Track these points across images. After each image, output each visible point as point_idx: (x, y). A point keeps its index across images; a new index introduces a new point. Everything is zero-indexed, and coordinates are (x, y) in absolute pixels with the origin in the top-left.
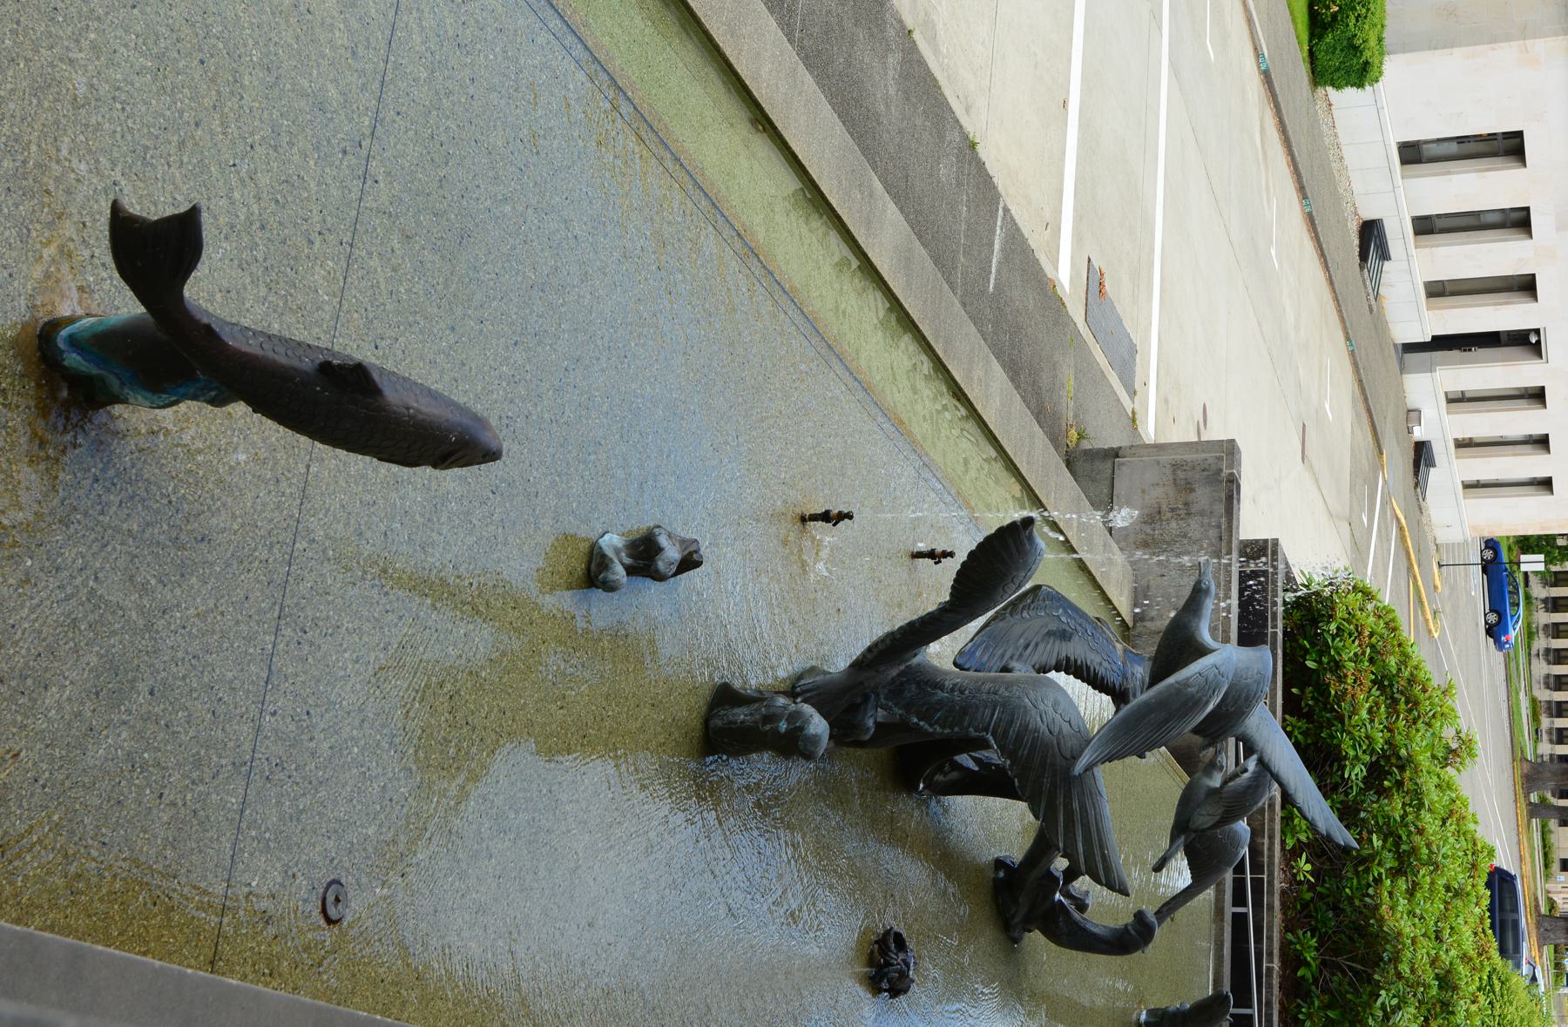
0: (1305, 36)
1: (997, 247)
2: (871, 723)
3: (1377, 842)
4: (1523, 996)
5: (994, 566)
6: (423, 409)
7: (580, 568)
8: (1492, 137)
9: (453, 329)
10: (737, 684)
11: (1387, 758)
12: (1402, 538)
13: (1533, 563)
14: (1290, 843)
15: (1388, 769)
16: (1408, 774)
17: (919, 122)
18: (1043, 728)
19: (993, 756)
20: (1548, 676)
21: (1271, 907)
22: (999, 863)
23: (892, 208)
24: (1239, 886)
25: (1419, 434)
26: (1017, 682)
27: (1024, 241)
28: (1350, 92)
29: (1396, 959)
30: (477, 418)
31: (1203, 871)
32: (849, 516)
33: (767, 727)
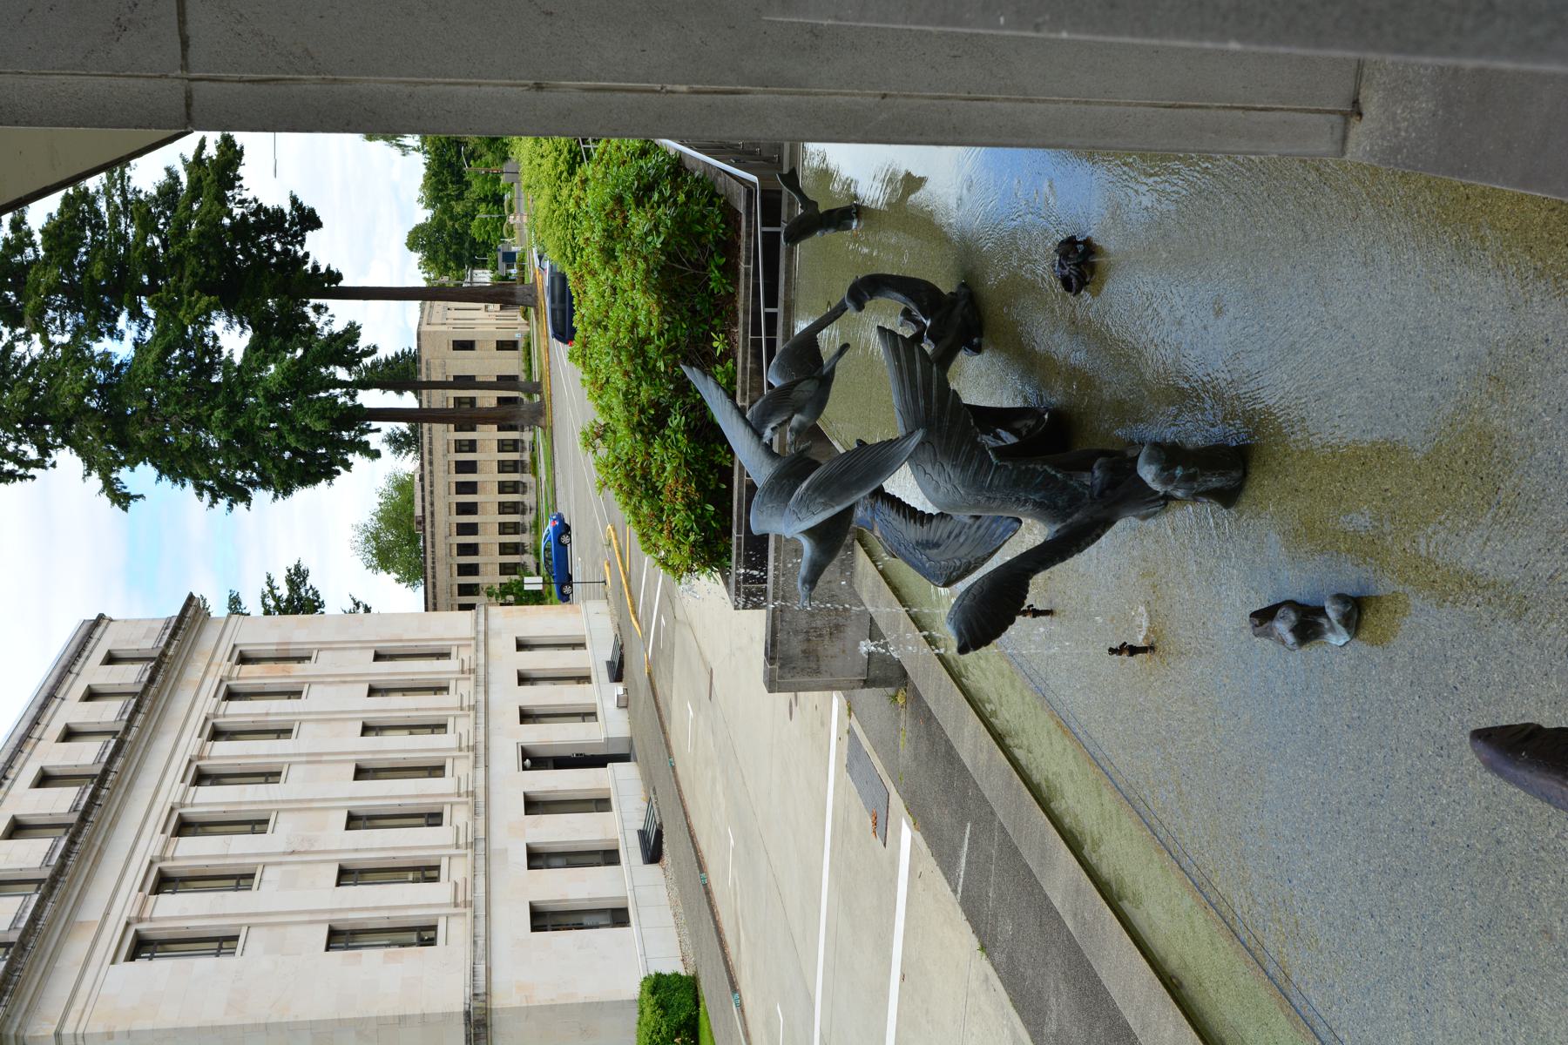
0: (702, 1019)
1: (963, 861)
2: (1097, 473)
3: (661, 365)
4: (549, 244)
5: (992, 612)
6: (1556, 785)
7: (1368, 615)
8: (556, 928)
9: (1498, 842)
10: (1217, 506)
11: (651, 431)
12: (634, 605)
13: (533, 583)
14: (729, 364)
15: (650, 424)
16: (635, 419)
17: (1030, 972)
18: (948, 468)
19: (988, 441)
20: (524, 492)
21: (746, 312)
22: (978, 350)
23: (1057, 903)
24: (772, 329)
25: (619, 689)
26: (970, 507)
27: (940, 864)
28: (667, 971)
29: (648, 272)
30: (1500, 773)
31: (809, 341)
32: (1112, 651)
33: (1192, 470)
